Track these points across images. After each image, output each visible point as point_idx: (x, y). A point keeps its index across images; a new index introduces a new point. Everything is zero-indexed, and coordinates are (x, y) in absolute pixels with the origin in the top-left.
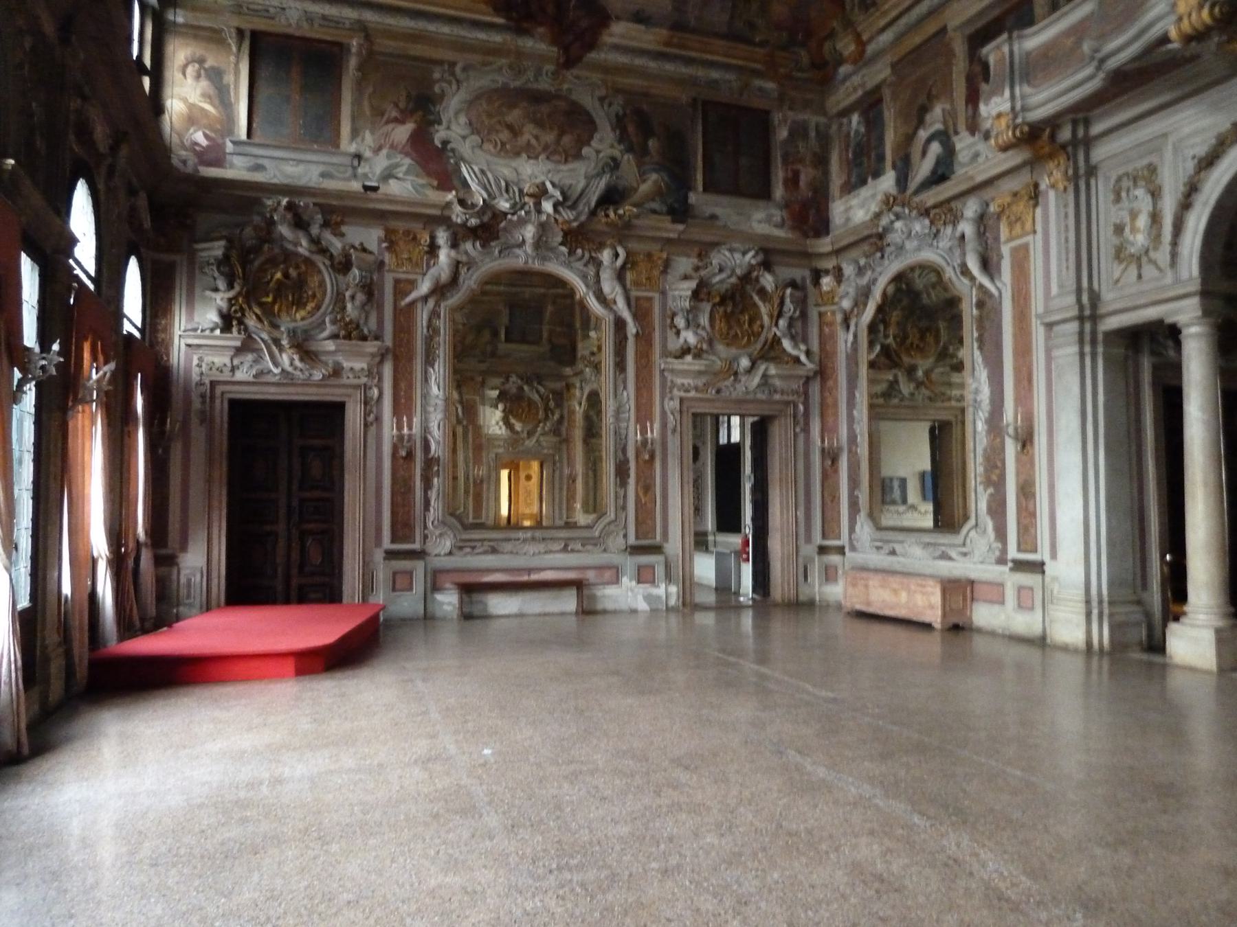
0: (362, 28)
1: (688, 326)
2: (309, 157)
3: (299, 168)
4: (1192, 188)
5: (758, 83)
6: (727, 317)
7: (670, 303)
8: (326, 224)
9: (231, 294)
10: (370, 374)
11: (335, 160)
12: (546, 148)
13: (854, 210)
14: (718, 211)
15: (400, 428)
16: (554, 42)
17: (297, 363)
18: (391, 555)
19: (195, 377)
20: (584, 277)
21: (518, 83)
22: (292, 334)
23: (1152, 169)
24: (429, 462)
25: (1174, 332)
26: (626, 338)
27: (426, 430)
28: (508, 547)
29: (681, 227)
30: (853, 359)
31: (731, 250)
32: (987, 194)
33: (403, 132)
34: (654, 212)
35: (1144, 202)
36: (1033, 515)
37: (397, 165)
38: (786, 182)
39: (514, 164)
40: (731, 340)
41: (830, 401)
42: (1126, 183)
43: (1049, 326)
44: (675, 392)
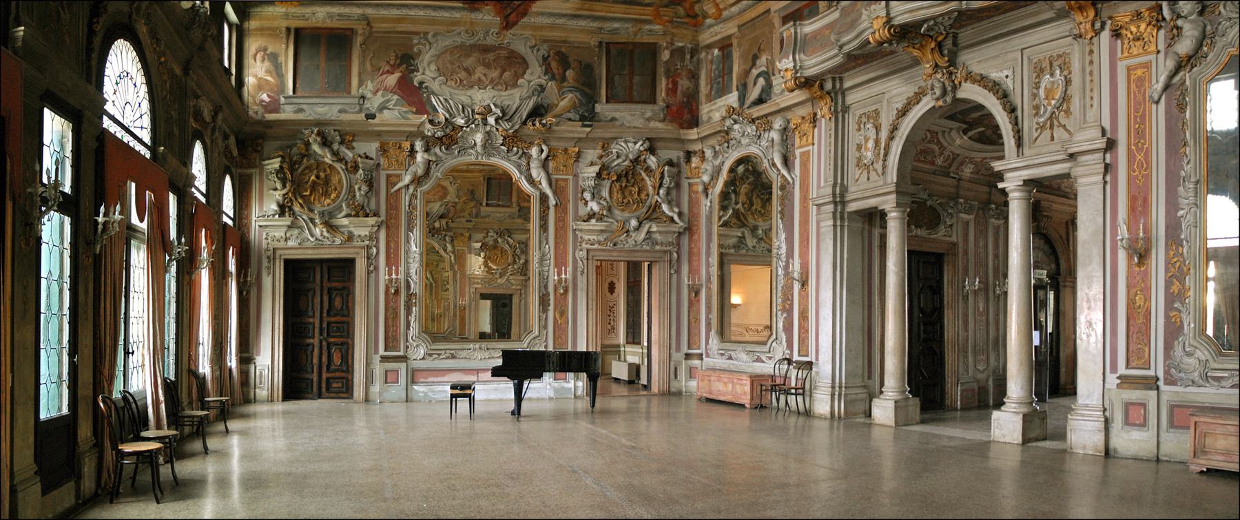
0: (368, 21)
1: (593, 197)
2: (331, 101)
3: (327, 109)
4: (894, 128)
5: (648, 27)
6: (622, 189)
7: (580, 183)
8: (342, 143)
9: (285, 191)
10: (371, 239)
11: (347, 101)
12: (492, 81)
13: (714, 111)
14: (617, 115)
15: (390, 274)
16: (497, 14)
17: (325, 234)
18: (384, 359)
19: (264, 246)
20: (519, 167)
21: (471, 42)
22: (322, 214)
23: (877, 112)
24: (410, 296)
25: (883, 214)
26: (548, 208)
27: (407, 274)
28: (464, 354)
29: (588, 129)
30: (709, 218)
31: (626, 142)
32: (789, 115)
33: (392, 80)
34: (570, 120)
35: (872, 133)
36: (807, 331)
37: (388, 101)
38: (668, 90)
39: (470, 92)
40: (625, 206)
41: (695, 250)
42: (864, 120)
43: (819, 206)
44: (584, 245)
